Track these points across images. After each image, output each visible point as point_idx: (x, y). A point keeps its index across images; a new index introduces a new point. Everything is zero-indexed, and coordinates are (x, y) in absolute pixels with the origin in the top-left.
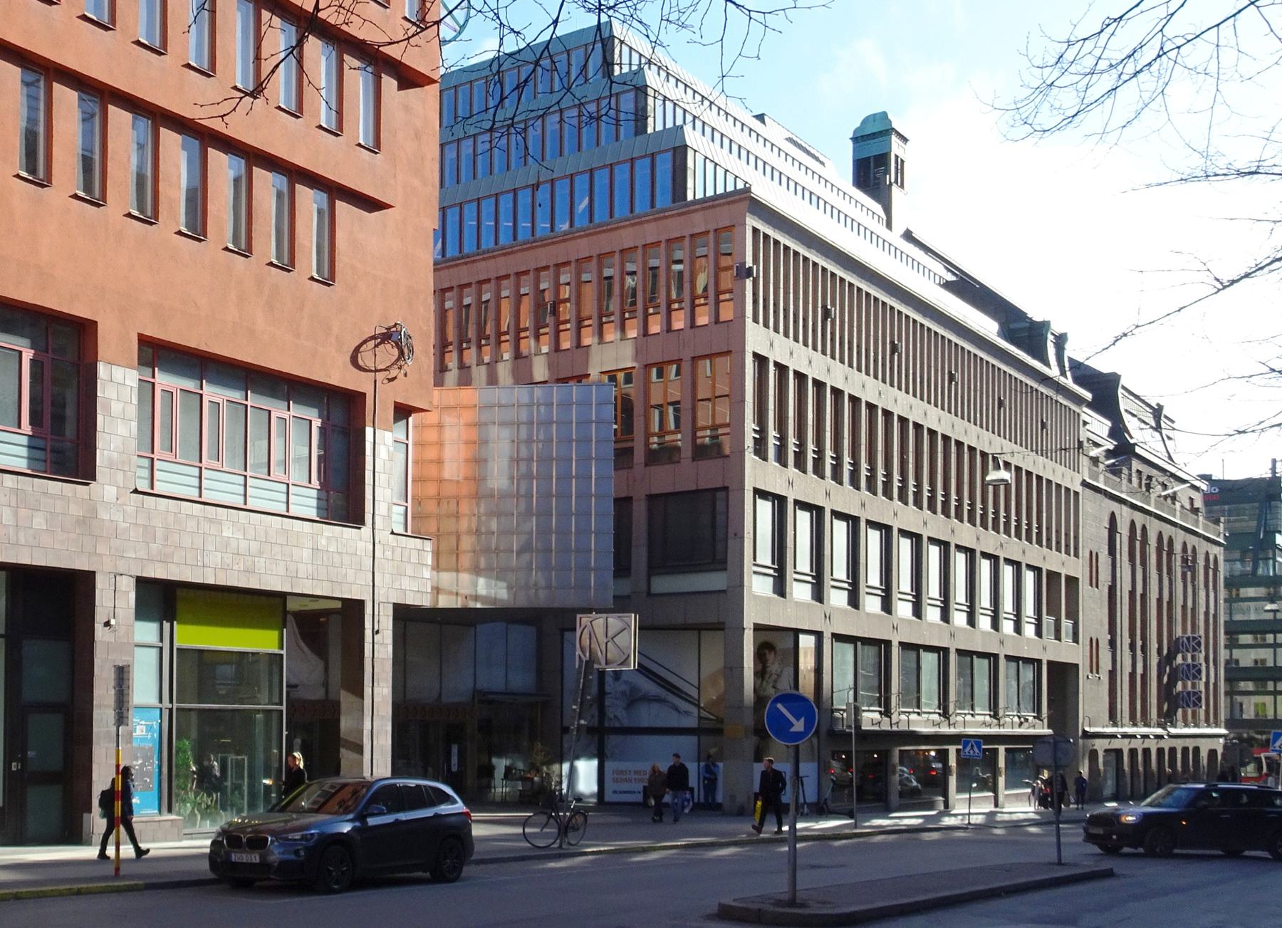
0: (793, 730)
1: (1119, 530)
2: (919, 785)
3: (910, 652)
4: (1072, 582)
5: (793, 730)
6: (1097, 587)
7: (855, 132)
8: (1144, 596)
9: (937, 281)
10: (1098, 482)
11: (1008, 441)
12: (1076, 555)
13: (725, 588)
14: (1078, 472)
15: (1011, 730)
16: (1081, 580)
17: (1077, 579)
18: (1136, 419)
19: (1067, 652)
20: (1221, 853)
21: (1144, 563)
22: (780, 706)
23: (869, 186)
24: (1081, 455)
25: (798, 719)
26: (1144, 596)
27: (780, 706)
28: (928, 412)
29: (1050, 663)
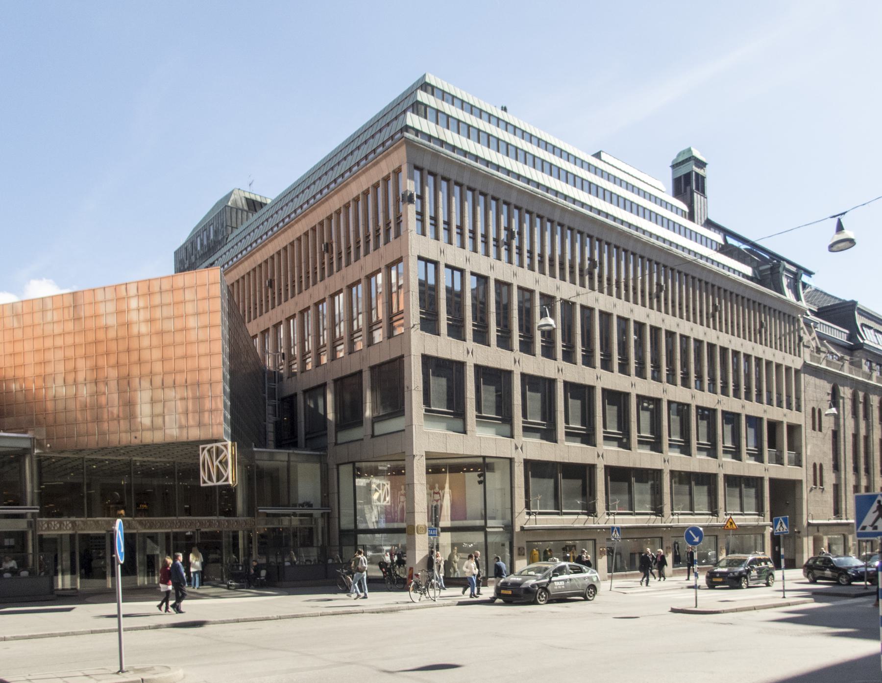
0: (695, 541)
1: (842, 395)
2: (170, 566)
3: (734, 489)
4: (793, 429)
5: (695, 541)
6: (820, 430)
7: (673, 162)
8: (867, 438)
9: (714, 247)
10: (844, 372)
11: (769, 347)
12: (798, 409)
13: (362, 437)
14: (799, 356)
15: (763, 523)
16: (803, 426)
17: (799, 426)
18: (872, 331)
19: (787, 472)
20: (728, 586)
21: (866, 416)
22: (690, 532)
23: (681, 193)
24: (802, 347)
25: (697, 537)
26: (867, 438)
27: (690, 532)
28: (766, 351)
29: (772, 481)
